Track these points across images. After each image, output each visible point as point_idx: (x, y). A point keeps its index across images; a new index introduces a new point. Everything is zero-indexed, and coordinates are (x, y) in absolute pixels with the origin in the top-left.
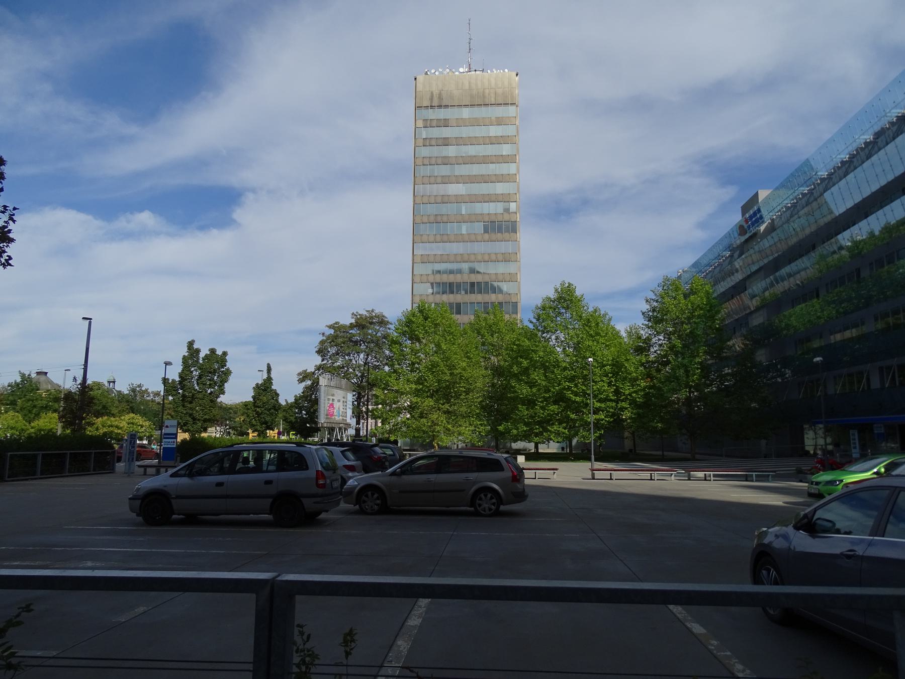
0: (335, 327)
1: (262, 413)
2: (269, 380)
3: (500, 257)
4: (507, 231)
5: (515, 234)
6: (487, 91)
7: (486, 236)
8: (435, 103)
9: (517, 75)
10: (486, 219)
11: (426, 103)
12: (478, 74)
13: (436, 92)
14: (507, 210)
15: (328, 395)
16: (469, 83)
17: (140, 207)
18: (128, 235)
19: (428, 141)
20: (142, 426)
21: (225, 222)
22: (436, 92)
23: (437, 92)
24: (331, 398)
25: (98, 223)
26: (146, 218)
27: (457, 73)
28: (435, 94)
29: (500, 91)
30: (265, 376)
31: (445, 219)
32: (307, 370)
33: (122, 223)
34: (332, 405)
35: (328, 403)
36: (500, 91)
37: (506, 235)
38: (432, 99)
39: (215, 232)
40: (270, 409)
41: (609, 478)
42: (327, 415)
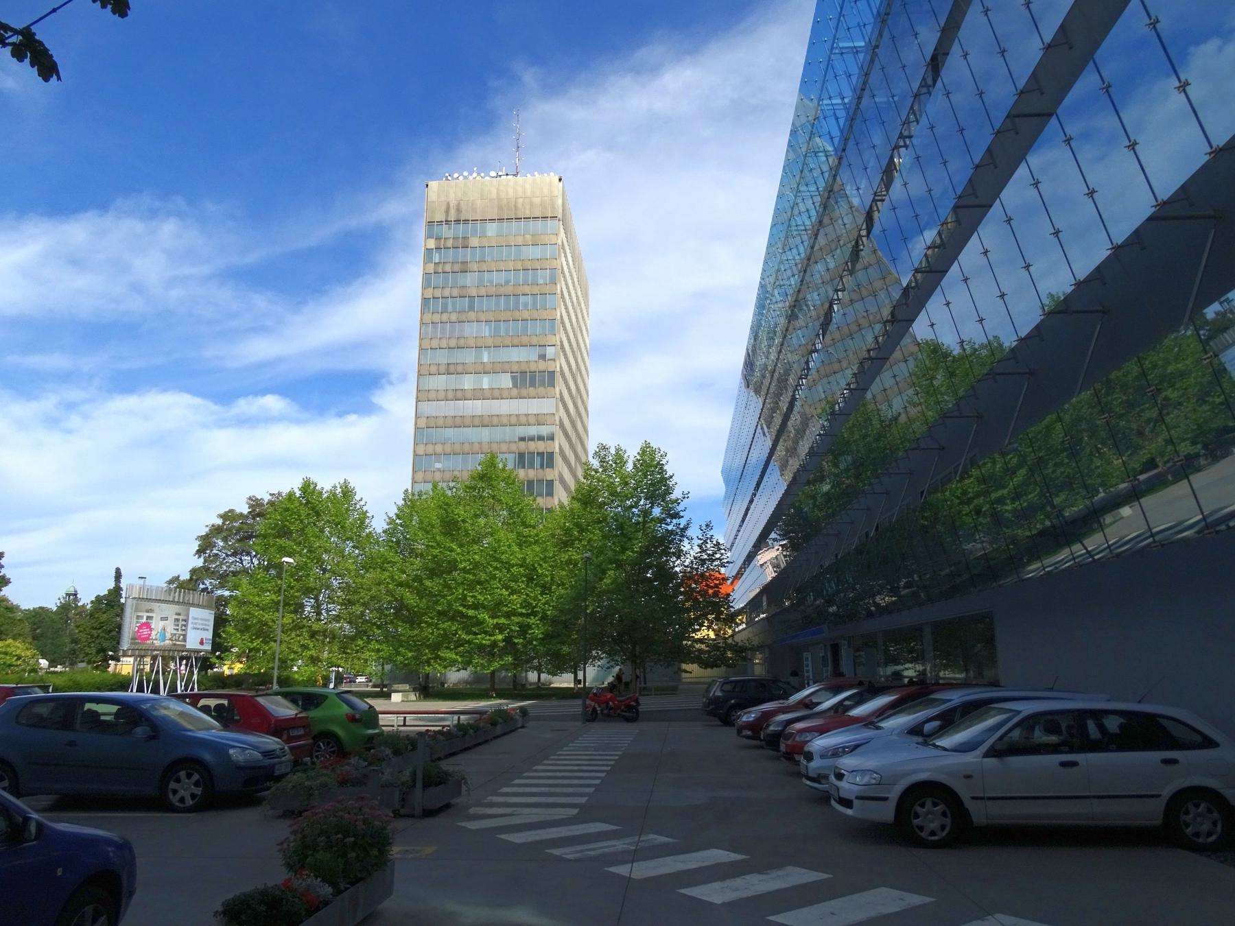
0: (228, 516)
1: (98, 636)
2: (117, 591)
3: (532, 420)
4: (542, 384)
5: (552, 388)
6: (520, 201)
7: (515, 392)
8: (452, 217)
9: (560, 180)
10: (515, 368)
11: (440, 217)
12: (510, 180)
13: (453, 203)
14: (543, 357)
15: (136, 610)
16: (498, 190)
17: (264, 392)
18: (246, 422)
19: (441, 266)
20: (19, 658)
21: (368, 409)
22: (453, 203)
23: (456, 203)
24: (145, 615)
25: (215, 408)
26: (272, 402)
27: (487, 178)
28: (451, 205)
29: (537, 201)
30: (112, 585)
31: (460, 369)
32: (179, 576)
33: (243, 406)
34: (147, 625)
35: (137, 622)
36: (537, 201)
37: (541, 390)
38: (447, 212)
39: (353, 417)
40: (110, 631)
41: (402, 724)
42: (132, 639)
